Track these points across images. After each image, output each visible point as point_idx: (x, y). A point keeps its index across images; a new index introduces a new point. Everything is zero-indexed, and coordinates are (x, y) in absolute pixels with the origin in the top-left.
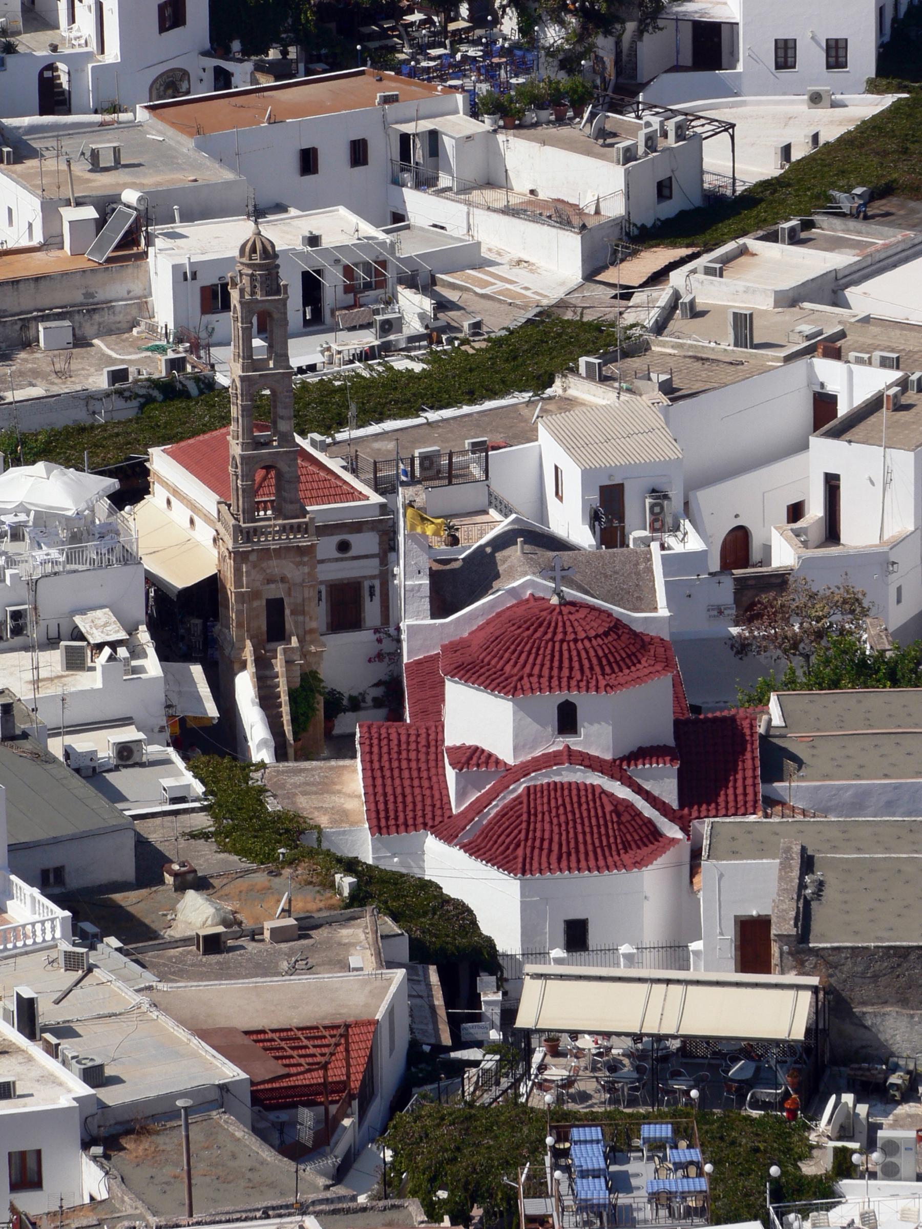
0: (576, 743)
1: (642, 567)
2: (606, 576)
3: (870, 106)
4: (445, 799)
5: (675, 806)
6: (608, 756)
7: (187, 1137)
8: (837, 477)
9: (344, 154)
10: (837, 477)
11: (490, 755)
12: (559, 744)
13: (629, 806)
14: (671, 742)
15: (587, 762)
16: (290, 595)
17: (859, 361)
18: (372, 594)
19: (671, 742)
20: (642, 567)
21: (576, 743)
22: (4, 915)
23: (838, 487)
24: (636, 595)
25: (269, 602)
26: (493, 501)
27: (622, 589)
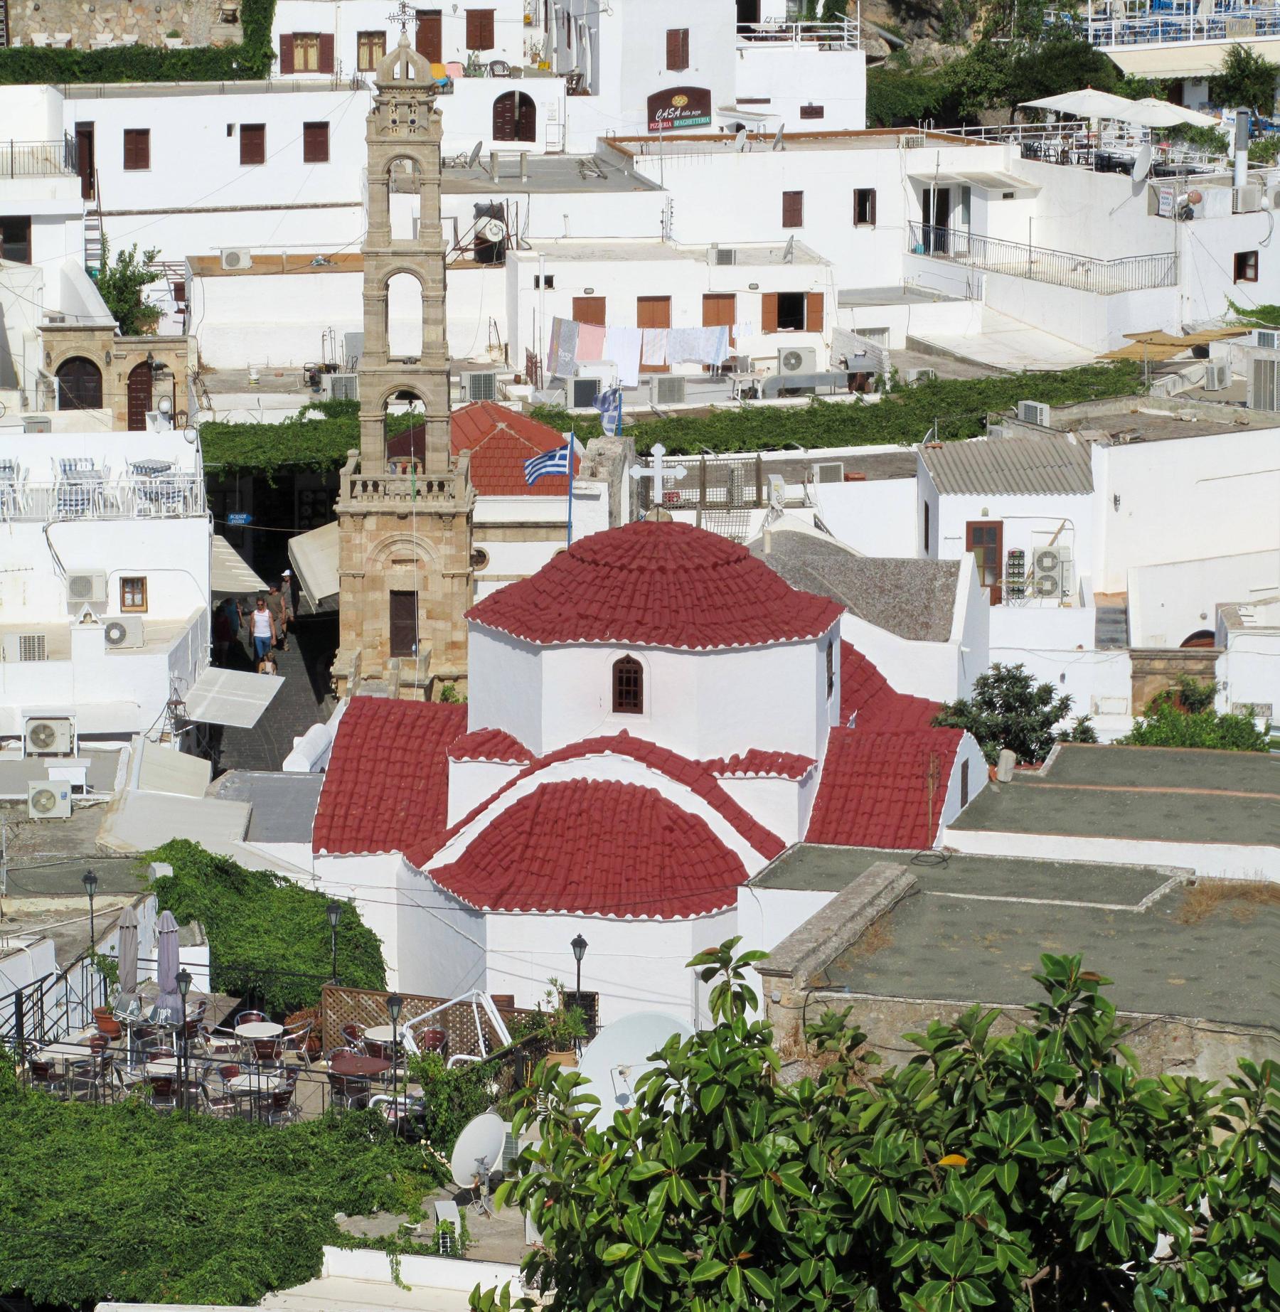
0: (635, 726)
1: (938, 584)
2: (882, 591)
13: (696, 825)
16: (425, 588)
21: (635, 726)
24: (922, 619)
25: (394, 594)
27: (902, 610)
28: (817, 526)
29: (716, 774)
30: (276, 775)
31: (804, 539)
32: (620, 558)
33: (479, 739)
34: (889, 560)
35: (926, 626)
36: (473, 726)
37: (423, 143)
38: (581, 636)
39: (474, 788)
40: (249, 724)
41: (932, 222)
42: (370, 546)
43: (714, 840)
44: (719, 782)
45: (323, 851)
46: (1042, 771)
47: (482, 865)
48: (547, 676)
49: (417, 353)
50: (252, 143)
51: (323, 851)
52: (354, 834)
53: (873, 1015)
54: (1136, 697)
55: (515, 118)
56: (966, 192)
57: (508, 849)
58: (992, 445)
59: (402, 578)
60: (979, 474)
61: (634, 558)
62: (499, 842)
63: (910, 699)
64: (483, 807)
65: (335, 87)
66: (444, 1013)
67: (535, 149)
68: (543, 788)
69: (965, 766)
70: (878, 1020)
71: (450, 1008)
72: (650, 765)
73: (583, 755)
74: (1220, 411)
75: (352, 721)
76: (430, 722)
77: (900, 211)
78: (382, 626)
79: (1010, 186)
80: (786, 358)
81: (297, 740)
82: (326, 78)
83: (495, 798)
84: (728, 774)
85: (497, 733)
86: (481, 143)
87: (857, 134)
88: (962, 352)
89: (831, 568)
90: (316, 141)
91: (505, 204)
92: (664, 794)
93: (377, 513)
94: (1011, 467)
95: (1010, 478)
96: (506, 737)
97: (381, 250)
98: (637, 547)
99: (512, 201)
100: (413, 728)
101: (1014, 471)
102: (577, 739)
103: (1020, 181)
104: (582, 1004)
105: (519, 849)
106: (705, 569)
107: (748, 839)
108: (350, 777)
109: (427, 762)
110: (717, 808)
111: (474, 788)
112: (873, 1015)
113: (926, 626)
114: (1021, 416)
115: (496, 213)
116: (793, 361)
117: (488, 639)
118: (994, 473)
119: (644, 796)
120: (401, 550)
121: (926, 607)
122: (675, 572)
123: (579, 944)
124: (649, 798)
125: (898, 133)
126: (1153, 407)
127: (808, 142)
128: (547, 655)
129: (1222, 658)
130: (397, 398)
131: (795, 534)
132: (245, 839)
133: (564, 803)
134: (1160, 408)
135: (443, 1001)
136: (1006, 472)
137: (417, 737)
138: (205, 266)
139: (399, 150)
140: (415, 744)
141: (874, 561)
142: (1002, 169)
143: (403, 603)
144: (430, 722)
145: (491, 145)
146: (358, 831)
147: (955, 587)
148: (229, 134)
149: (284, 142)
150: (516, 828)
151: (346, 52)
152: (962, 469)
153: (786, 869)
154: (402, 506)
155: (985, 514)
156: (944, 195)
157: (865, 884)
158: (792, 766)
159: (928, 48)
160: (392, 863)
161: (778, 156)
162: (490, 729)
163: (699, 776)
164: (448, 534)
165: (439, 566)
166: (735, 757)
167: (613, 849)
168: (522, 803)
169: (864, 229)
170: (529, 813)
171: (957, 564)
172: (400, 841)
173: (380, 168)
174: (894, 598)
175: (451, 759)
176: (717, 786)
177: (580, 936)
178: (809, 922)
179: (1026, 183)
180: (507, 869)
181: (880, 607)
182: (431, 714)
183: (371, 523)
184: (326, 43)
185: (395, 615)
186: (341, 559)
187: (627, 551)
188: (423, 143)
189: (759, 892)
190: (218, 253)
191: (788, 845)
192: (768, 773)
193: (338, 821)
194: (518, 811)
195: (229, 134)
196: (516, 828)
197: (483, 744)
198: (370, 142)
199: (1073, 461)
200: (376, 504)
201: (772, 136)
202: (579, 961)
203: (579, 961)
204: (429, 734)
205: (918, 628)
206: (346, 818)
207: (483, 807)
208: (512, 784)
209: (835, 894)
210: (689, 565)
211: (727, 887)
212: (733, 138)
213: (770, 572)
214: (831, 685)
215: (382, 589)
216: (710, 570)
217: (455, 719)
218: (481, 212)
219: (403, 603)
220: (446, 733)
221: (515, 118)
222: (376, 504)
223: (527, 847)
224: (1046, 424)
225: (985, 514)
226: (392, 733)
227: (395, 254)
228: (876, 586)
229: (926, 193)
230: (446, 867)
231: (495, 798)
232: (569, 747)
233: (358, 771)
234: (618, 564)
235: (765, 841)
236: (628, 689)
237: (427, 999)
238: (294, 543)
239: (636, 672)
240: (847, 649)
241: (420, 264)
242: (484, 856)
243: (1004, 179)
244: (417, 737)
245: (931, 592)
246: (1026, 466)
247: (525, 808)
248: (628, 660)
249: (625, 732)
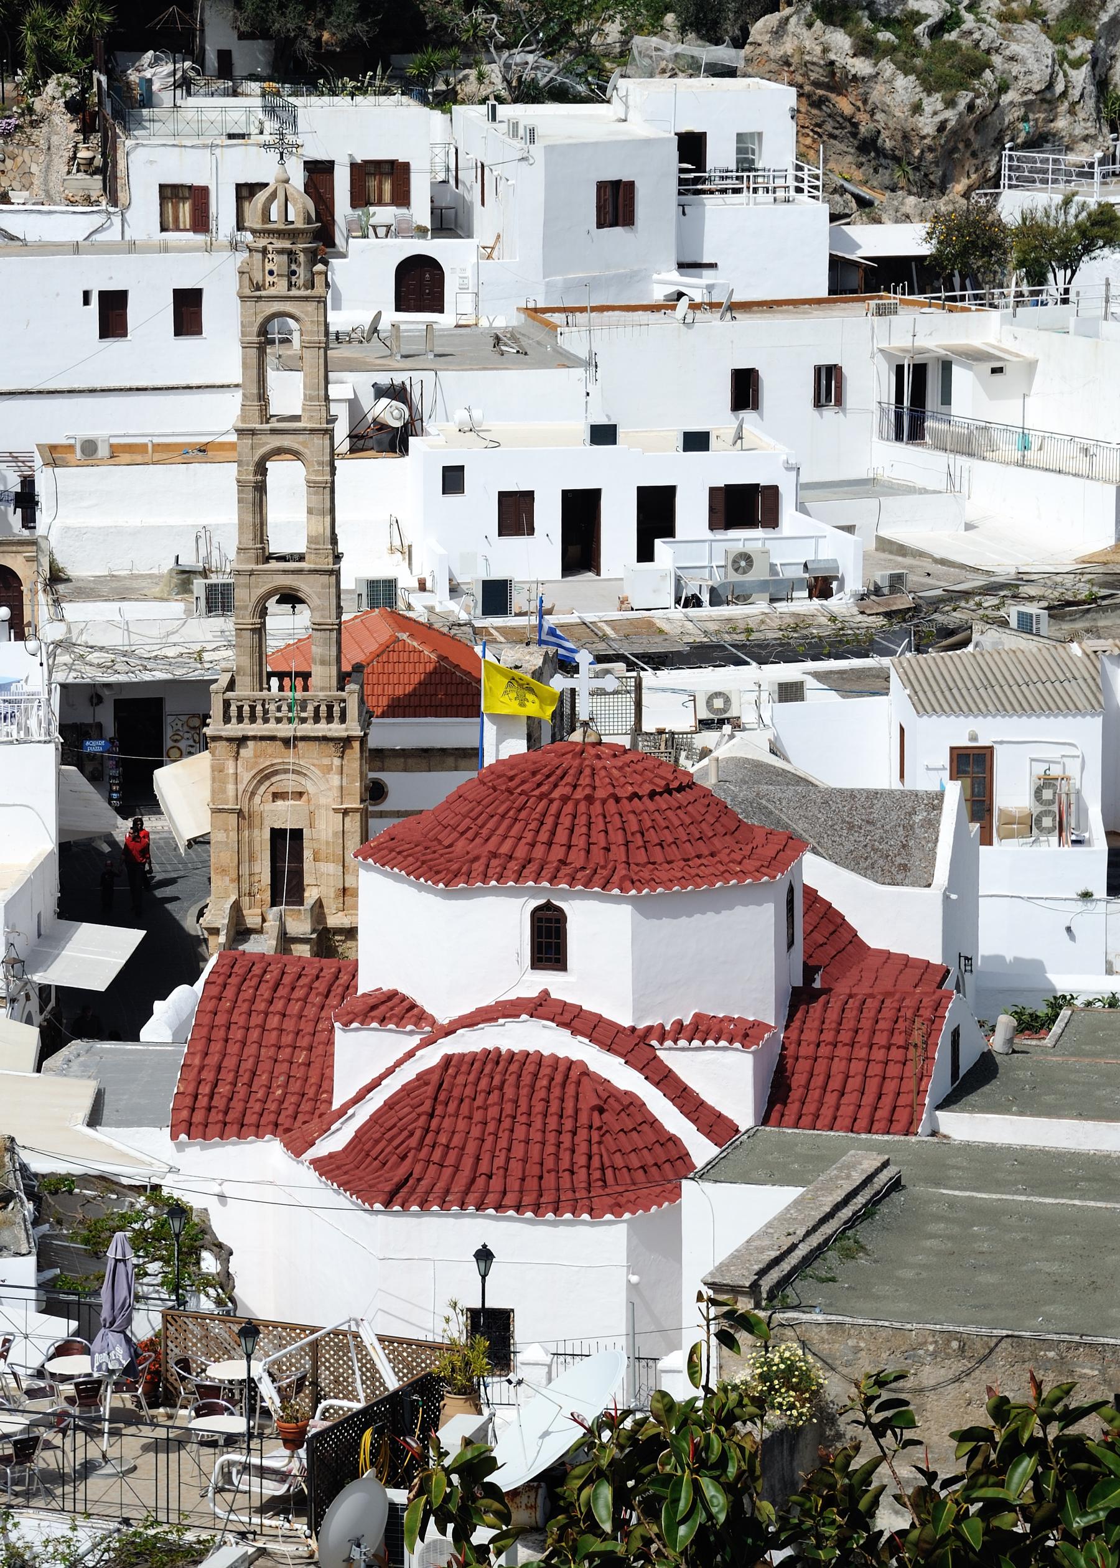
0: (558, 985)
1: (917, 819)
2: (851, 827)
4: (325, 1086)
6: (625, 1020)
9: (769, 389)
11: (413, 1006)
13: (631, 1104)
15: (567, 1017)
21: (558, 985)
24: (899, 860)
27: (875, 850)
28: (772, 751)
29: (654, 1043)
30: (130, 1046)
31: (758, 767)
32: (539, 785)
33: (372, 1001)
34: (859, 791)
35: (905, 868)
36: (365, 985)
37: (306, 299)
38: (491, 878)
39: (365, 1064)
40: (102, 988)
41: (906, 402)
43: (653, 1123)
44: (658, 1053)
46: (1048, 1041)
47: (374, 1153)
49: (301, 548)
50: (113, 312)
51: (183, 1137)
52: (220, 1117)
53: (850, 1343)
55: (419, 284)
56: (946, 367)
57: (405, 1133)
58: (979, 658)
60: (964, 691)
61: (556, 786)
62: (394, 1126)
63: (887, 955)
64: (376, 1083)
65: (209, 249)
66: (315, 1345)
67: (444, 321)
68: (448, 1060)
69: (956, 1034)
70: (857, 1350)
71: (323, 1338)
73: (496, 1020)
75: (220, 981)
76: (313, 982)
77: (871, 388)
79: (1000, 359)
80: (734, 562)
81: (158, 1005)
82: (200, 238)
83: (390, 1072)
84: (669, 1043)
85: (393, 995)
86: (380, 313)
87: (819, 301)
88: (939, 554)
89: (790, 801)
90: (187, 310)
91: (407, 383)
94: (1003, 682)
95: (1001, 695)
96: (404, 998)
97: (258, 426)
98: (559, 772)
99: (421, 381)
100: (293, 989)
101: (1006, 688)
102: (488, 1001)
103: (1010, 353)
104: (492, 1329)
105: (418, 1133)
106: (640, 798)
107: (694, 1121)
108: (216, 1047)
109: (310, 1029)
110: (657, 1084)
111: (365, 1064)
112: (850, 1343)
113: (905, 868)
114: (1014, 623)
115: (398, 393)
116: (743, 564)
118: (982, 691)
119: (569, 1069)
120: (288, 783)
121: (904, 846)
122: (604, 802)
123: (484, 1256)
124: (572, 1073)
125: (863, 300)
127: (762, 312)
130: (278, 602)
131: (747, 760)
132: (94, 1119)
133: (472, 1078)
135: (314, 1330)
136: (997, 688)
137: (298, 1000)
138: (55, 455)
139: (277, 307)
140: (294, 1008)
141: (841, 792)
144: (313, 982)
145: (391, 316)
146: (226, 1113)
147: (939, 822)
148: (86, 302)
149: (150, 313)
150: (414, 1108)
151: (223, 208)
152: (943, 685)
153: (737, 1155)
154: (285, 730)
156: (920, 371)
157: (837, 1177)
158: (742, 1033)
159: (902, 204)
160: (268, 1152)
161: (728, 323)
162: (385, 989)
163: (635, 1046)
166: (679, 1023)
167: (514, 1136)
168: (422, 1078)
170: (430, 1090)
171: (940, 796)
172: (276, 1125)
173: (255, 329)
174: (866, 836)
175: (337, 1025)
176: (655, 1057)
177: (485, 1246)
178: (769, 1225)
179: (1018, 355)
180: (403, 1158)
181: (849, 846)
182: (315, 972)
183: (250, 748)
184: (199, 196)
186: (213, 792)
187: (548, 776)
188: (306, 299)
189: (708, 1186)
190: (72, 441)
191: (742, 1129)
192: (717, 1041)
193: (203, 1101)
194: (419, 1087)
195: (86, 302)
196: (414, 1108)
197: (373, 1008)
198: (243, 298)
199: (1077, 675)
201: (719, 305)
202: (484, 1277)
203: (484, 1277)
204: (312, 996)
205: (894, 870)
206: (211, 1098)
207: (376, 1083)
208: (410, 1054)
209: (800, 1190)
210: (620, 793)
211: (670, 1181)
212: (674, 308)
213: (718, 802)
214: (791, 944)
216: (646, 799)
217: (344, 978)
218: (381, 392)
220: (332, 994)
221: (419, 284)
223: (427, 1131)
225: (974, 738)
226: (267, 995)
227: (274, 431)
228: (844, 821)
229: (900, 369)
230: (331, 1156)
231: (390, 1072)
232: (479, 1011)
233: (227, 1041)
234: (537, 792)
235: (714, 1125)
236: (549, 943)
237: (293, 1327)
238: (159, 774)
239: (558, 921)
240: (811, 894)
241: (303, 444)
242: (377, 1142)
243: (992, 351)
244: (298, 1000)
245: (909, 828)
246: (1021, 682)
247: (426, 1084)
248: (548, 906)
249: (546, 993)
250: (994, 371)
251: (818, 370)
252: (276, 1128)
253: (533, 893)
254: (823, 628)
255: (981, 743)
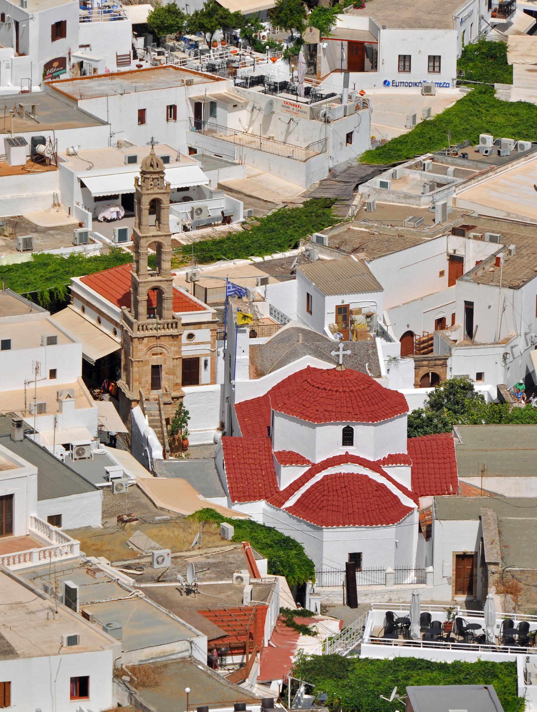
0: (351, 450)
1: (370, 352)
3: (457, 93)
5: (410, 489)
7: (32, 590)
8: (472, 304)
10: (472, 304)
12: (342, 450)
13: (382, 487)
14: (404, 451)
16: (165, 364)
17: (475, 238)
18: (206, 365)
19: (404, 451)
20: (370, 352)
22: (301, 634)
23: (472, 309)
25: (153, 367)
26: (273, 312)
27: (360, 364)
37: (164, 193)
42: (145, 349)
45: (236, 502)
48: (318, 435)
54: (416, 376)
59: (156, 360)
70: (527, 577)
72: (365, 467)
74: (390, 229)
77: (186, 112)
78: (148, 378)
92: (370, 477)
93: (148, 337)
117: (287, 421)
120: (159, 350)
126: (357, 227)
128: (318, 429)
129: (450, 359)
134: (360, 227)
142: (226, 91)
143: (156, 370)
155: (343, 302)
163: (376, 466)
164: (175, 343)
165: (171, 355)
169: (172, 123)
185: (153, 373)
200: (147, 333)
215: (148, 365)
219: (156, 370)
222: (147, 333)
224: (327, 245)
225: (343, 302)
236: (348, 438)
241: (163, 240)
250: (234, 106)
251: (167, 107)
252: (266, 498)
253: (343, 424)
254: (230, 237)
255: (344, 304)
